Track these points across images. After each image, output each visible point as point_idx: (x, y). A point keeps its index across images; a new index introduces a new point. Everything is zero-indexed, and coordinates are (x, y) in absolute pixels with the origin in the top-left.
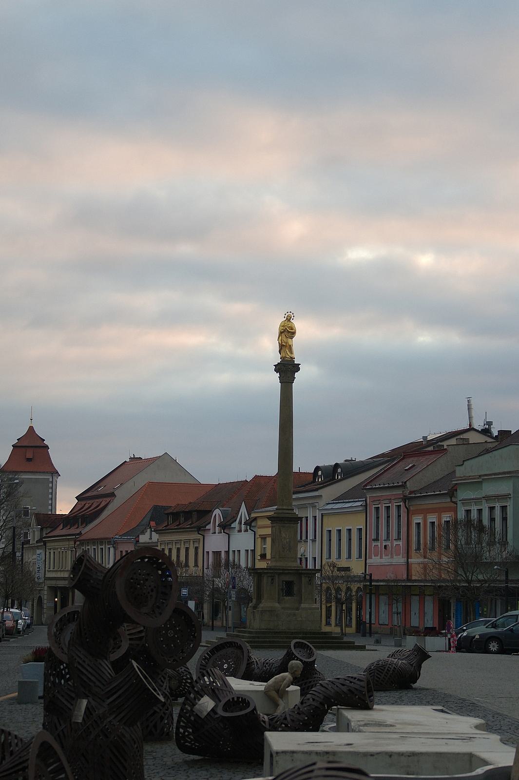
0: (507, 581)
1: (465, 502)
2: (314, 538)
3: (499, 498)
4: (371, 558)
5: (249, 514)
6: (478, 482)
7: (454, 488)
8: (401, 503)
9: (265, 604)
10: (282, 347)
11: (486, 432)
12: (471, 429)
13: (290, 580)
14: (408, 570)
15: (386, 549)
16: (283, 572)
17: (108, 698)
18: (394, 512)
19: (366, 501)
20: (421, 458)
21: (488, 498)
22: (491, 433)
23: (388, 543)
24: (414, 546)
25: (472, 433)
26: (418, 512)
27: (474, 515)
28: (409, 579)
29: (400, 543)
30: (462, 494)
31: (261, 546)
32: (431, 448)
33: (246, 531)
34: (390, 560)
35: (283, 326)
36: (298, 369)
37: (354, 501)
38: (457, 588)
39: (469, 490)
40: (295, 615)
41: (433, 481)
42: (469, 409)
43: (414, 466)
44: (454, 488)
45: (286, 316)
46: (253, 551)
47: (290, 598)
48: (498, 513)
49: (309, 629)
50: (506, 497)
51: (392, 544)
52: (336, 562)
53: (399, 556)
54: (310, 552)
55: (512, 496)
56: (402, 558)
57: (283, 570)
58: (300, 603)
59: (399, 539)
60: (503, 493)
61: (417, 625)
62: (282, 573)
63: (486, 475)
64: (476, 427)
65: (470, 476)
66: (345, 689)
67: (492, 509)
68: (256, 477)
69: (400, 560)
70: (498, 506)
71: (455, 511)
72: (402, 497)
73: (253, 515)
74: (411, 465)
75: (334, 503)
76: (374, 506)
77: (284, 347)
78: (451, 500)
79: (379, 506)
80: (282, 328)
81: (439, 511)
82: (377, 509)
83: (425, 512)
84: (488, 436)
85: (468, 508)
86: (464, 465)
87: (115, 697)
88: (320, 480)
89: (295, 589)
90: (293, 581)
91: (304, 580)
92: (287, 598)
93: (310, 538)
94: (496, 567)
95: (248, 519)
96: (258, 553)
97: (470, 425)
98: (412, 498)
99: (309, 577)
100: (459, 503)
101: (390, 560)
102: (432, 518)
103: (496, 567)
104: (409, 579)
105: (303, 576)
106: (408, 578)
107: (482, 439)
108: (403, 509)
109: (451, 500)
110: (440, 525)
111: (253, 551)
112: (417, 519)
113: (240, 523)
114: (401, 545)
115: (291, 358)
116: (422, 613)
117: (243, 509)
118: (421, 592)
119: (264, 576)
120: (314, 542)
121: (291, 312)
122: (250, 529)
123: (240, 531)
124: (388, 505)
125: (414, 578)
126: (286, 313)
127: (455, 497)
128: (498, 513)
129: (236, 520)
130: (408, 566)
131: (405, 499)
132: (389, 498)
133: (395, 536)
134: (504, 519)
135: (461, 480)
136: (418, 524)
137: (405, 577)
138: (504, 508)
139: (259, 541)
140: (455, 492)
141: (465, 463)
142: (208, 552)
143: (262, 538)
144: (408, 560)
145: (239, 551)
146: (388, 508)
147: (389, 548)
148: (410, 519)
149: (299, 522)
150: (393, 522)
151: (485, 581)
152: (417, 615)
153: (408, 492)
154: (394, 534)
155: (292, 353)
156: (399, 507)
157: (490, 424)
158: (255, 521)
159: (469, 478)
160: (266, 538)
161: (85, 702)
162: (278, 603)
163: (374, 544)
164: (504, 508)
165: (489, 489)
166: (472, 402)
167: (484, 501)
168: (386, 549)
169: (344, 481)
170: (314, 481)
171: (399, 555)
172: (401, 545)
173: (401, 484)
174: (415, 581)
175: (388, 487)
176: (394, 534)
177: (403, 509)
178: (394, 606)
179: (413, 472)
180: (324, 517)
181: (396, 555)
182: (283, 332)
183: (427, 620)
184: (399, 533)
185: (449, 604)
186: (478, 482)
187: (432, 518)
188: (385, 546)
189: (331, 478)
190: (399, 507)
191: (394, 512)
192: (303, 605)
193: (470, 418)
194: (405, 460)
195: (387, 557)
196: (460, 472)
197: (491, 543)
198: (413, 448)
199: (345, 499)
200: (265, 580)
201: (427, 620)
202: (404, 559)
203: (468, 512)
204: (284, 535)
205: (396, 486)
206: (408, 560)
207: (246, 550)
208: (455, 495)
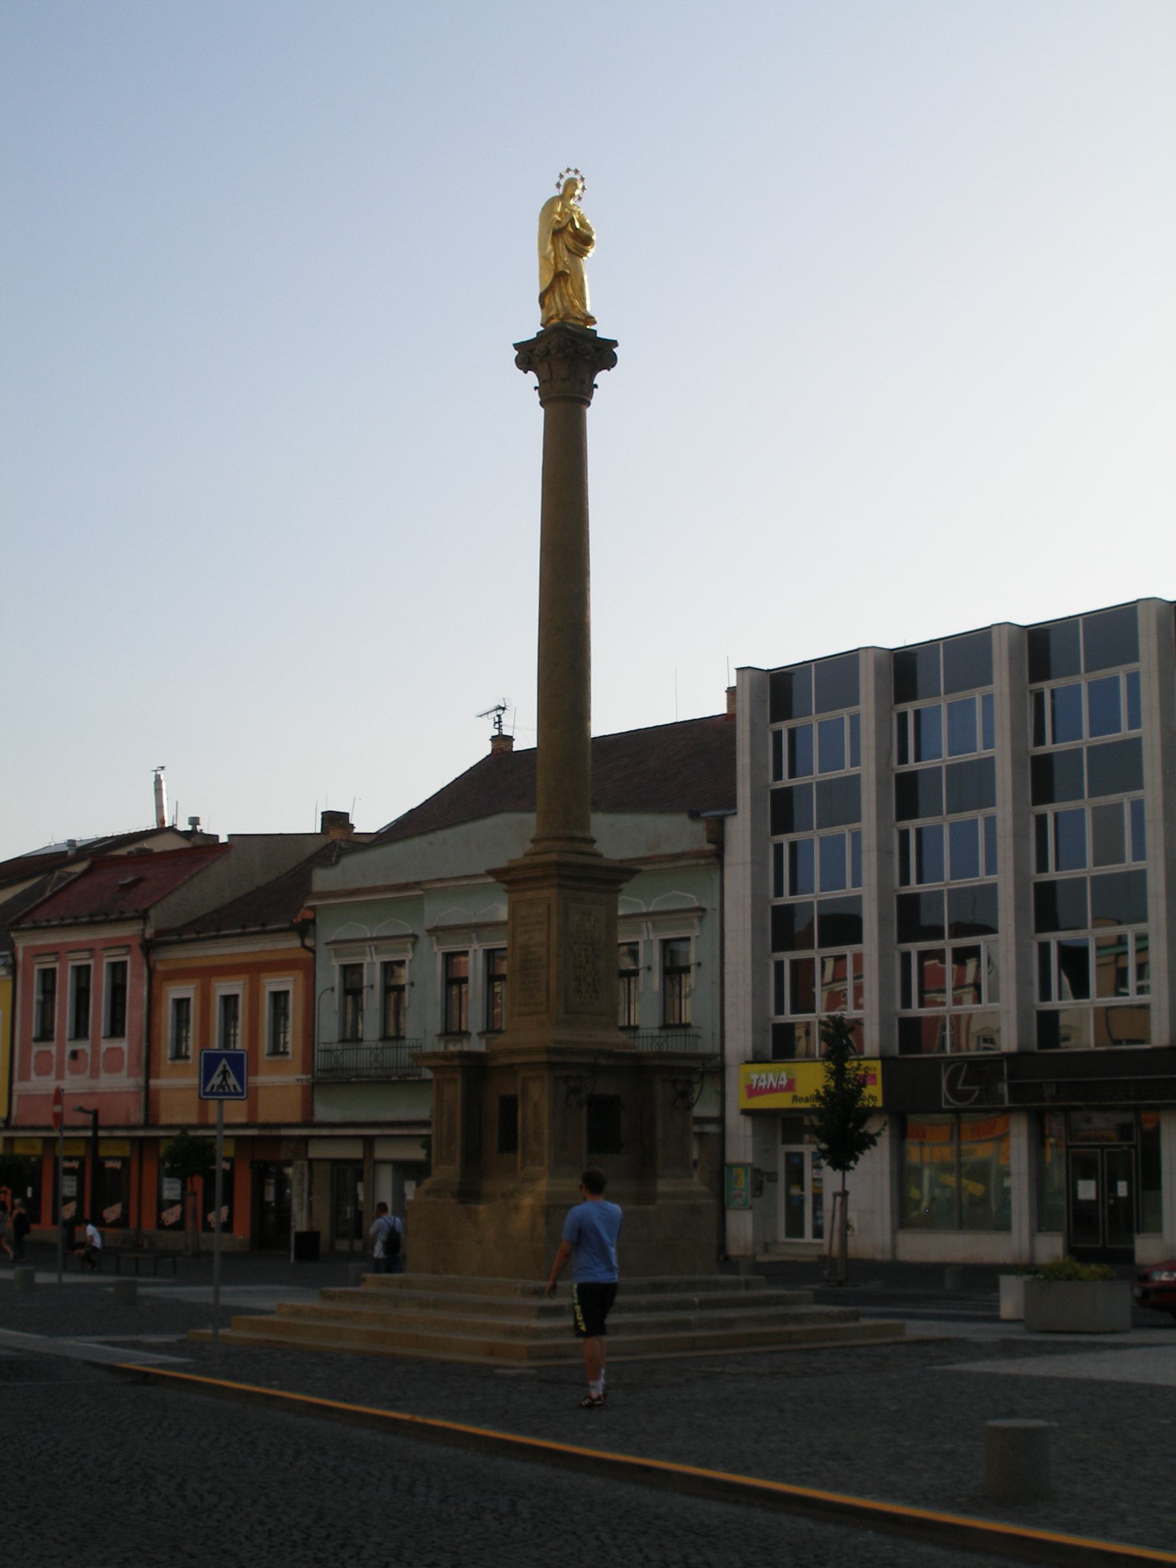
3: (478, 929)
4: (25, 1077)
19: (14, 956)
23: (84, 1046)
28: (149, 1124)
29: (123, 1044)
30: (329, 931)
45: (562, 182)
77: (561, 282)
112: (175, 991)
121: (568, 170)
126: (573, 168)
136: (181, 1004)
137: (138, 1117)
142: (116, 1029)
163: (36, 1048)
171: (48, 1073)
172: (960, 1082)
188: (74, 1055)
193: (159, 808)
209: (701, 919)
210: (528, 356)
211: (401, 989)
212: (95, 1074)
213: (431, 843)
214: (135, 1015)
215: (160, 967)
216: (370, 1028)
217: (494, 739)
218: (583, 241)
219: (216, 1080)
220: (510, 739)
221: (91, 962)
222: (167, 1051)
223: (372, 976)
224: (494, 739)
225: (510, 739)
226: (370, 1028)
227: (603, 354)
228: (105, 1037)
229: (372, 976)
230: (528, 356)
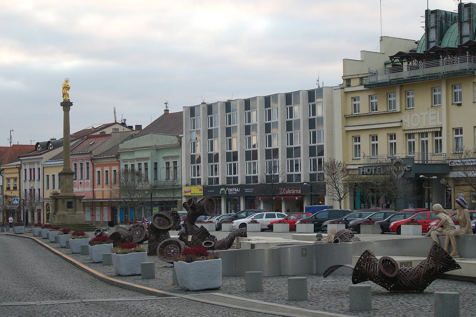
1: (124, 161)
6: (133, 151)
7: (118, 154)
8: (89, 162)
9: (60, 212)
11: (123, 124)
12: (116, 123)
14: (93, 194)
15: (81, 184)
16: (68, 197)
18: (85, 166)
21: (137, 159)
23: (82, 181)
24: (97, 182)
25: (117, 125)
26: (98, 166)
27: (129, 167)
29: (89, 181)
30: (122, 157)
32: (98, 133)
34: (84, 189)
35: (65, 85)
38: (126, 202)
41: (105, 151)
42: (115, 113)
43: (94, 143)
49: (80, 223)
50: (147, 159)
55: (150, 158)
58: (76, 211)
59: (88, 179)
64: (117, 121)
65: (127, 149)
66: (241, 232)
67: (139, 164)
69: (89, 189)
70: (143, 163)
72: (90, 158)
74: (92, 143)
75: (50, 161)
79: (77, 163)
80: (64, 86)
81: (111, 165)
82: (75, 164)
83: (103, 166)
84: (125, 126)
88: (39, 149)
89: (73, 205)
91: (77, 201)
92: (70, 209)
93: (36, 179)
94: (146, 192)
96: (5, 187)
97: (116, 121)
98: (95, 159)
101: (84, 189)
102: (106, 168)
104: (94, 198)
105: (77, 199)
107: (121, 129)
110: (120, 172)
112: (98, 169)
116: (102, 215)
118: (102, 204)
120: (39, 181)
124: (82, 162)
131: (92, 159)
132: (82, 159)
133: (86, 177)
134: (146, 169)
135: (122, 150)
136: (99, 172)
137: (92, 197)
138: (146, 164)
139: (5, 181)
142: (88, 179)
143: (7, 179)
144: (93, 189)
146: (81, 164)
147: (83, 184)
148: (94, 169)
151: (142, 198)
154: (85, 176)
157: (125, 120)
158: (3, 171)
161: (191, 236)
162: (66, 211)
164: (146, 164)
165: (138, 155)
168: (81, 184)
169: (55, 150)
170: (36, 150)
173: (89, 152)
175: (82, 154)
176: (85, 176)
178: (98, 213)
179: (95, 146)
180: (44, 168)
181: (86, 187)
182: (65, 88)
183: (105, 218)
184: (88, 176)
185: (117, 210)
186: (133, 151)
188: (80, 183)
189: (46, 148)
191: (85, 166)
192: (77, 212)
193: (115, 117)
194: (88, 140)
195: (81, 188)
197: (140, 180)
198: (86, 133)
200: (60, 202)
201: (105, 218)
203: (126, 166)
204: (67, 181)
206: (93, 189)
209: (178, 157)
212: (84, 188)
214: (91, 174)
215: (95, 164)
216: (171, 177)
219: (15, 202)
222: (97, 182)
223: (171, 165)
224: (165, 110)
226: (171, 177)
227: (71, 104)
229: (171, 165)
230: (62, 104)
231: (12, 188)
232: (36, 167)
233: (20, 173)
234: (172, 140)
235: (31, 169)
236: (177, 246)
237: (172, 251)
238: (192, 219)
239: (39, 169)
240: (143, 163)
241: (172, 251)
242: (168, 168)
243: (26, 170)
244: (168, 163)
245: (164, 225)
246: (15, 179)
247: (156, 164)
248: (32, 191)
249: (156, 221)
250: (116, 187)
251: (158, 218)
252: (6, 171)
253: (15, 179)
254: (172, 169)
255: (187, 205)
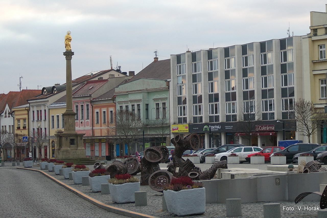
0: (143, 135)
1: (119, 103)
2: (37, 120)
3: (136, 101)
5: (10, 109)
6: (127, 94)
8: (89, 104)
9: (64, 148)
10: (66, 45)
11: (118, 71)
12: (112, 70)
13: (74, 138)
14: (93, 132)
17: (184, 167)
18: (85, 108)
20: (95, 84)
21: (131, 101)
22: (120, 71)
23: (83, 121)
24: (95, 122)
26: (97, 107)
27: (124, 108)
29: (89, 121)
31: (17, 123)
33: (9, 117)
34: (84, 128)
35: (67, 37)
36: (73, 54)
37: (60, 103)
38: (121, 139)
39: (121, 98)
40: (76, 152)
42: (111, 61)
43: (93, 87)
44: (114, 97)
46: (13, 126)
47: (73, 145)
48: (136, 107)
50: (139, 100)
51: (85, 121)
52: (62, 130)
53: (88, 126)
54: (43, 126)
56: (90, 127)
57: (71, 134)
58: (77, 147)
59: (88, 119)
60: (138, 99)
61: (98, 155)
62: (70, 136)
63: (130, 91)
64: (113, 68)
65: (122, 92)
67: (133, 105)
68: (10, 92)
69: (89, 128)
70: (136, 104)
71: (115, 106)
73: (13, 110)
74: (91, 87)
76: (75, 105)
78: (113, 102)
79: (78, 105)
81: (107, 106)
83: (101, 107)
84: (120, 73)
85: (121, 105)
86: (119, 87)
87: (185, 166)
88: (45, 93)
89: (75, 142)
90: (74, 139)
91: (79, 138)
92: (72, 146)
94: (139, 130)
95: (10, 111)
96: (16, 127)
99: (81, 137)
100: (117, 103)
101: (84, 128)
102: (104, 110)
103: (139, 130)
104: (93, 136)
105: (78, 137)
106: (93, 136)
108: (90, 106)
109: (113, 102)
111: (13, 126)
112: (97, 110)
113: (6, 113)
114: (89, 121)
115: (70, 50)
116: (100, 150)
117: (7, 107)
118: (100, 141)
119: (63, 137)
122: (12, 116)
123: (6, 117)
125: (95, 135)
127: (115, 101)
128: (136, 107)
129: (3, 112)
130: (93, 130)
131: (91, 102)
132: (83, 101)
134: (139, 110)
136: (97, 112)
137: (91, 135)
138: (138, 105)
139: (16, 121)
140: (115, 99)
141: (119, 86)
142: (53, 116)
145: (5, 126)
146: (82, 106)
148: (93, 110)
149: (76, 115)
150: (85, 112)
151: (135, 135)
152: (98, 151)
153: (92, 99)
154: (85, 116)
155: (70, 48)
156: (88, 105)
157: (120, 67)
159: (121, 92)
160: (20, 120)
164: (138, 105)
165: (132, 97)
166: (112, 58)
167: (129, 102)
170: (42, 94)
171: (88, 126)
172: (89, 121)
173: (89, 95)
174: (96, 137)
176: (85, 116)
177: (90, 106)
178: (97, 148)
181: (87, 126)
184: (88, 116)
186: (127, 94)
187: (104, 110)
188: (81, 122)
190: (88, 105)
191: (85, 108)
193: (111, 65)
196: (117, 90)
197: (133, 120)
199: (60, 102)
200: (64, 139)
201: (103, 153)
202: (91, 127)
203: (121, 107)
204: (70, 121)
205: (79, 97)
207: (9, 126)
208: (115, 100)
209: (167, 99)
210: (65, 54)
211: (159, 109)
212: (85, 127)
213: (131, 84)
214: (90, 115)
215: (94, 106)
216: (161, 117)
217: (154, 58)
218: (70, 40)
219: (24, 139)
220: (158, 58)
221: (83, 104)
222: (95, 122)
223: (161, 106)
225: (158, 58)
226: (161, 117)
227: (73, 54)
228: (86, 119)
229: (161, 106)
230: (65, 54)
231: (21, 128)
232: (43, 109)
233: (28, 114)
234: (161, 84)
235: (38, 111)
236: (166, 177)
237: (162, 181)
238: (179, 153)
239: (45, 110)
240: (136, 104)
241: (162, 181)
242: (158, 109)
243: (34, 112)
244: (158, 104)
245: (155, 158)
246: (24, 120)
247: (147, 105)
248: (39, 129)
249: (148, 155)
250: (113, 126)
251: (149, 152)
252: (16, 113)
253: (24, 120)
254: (161, 110)
255: (175, 140)
